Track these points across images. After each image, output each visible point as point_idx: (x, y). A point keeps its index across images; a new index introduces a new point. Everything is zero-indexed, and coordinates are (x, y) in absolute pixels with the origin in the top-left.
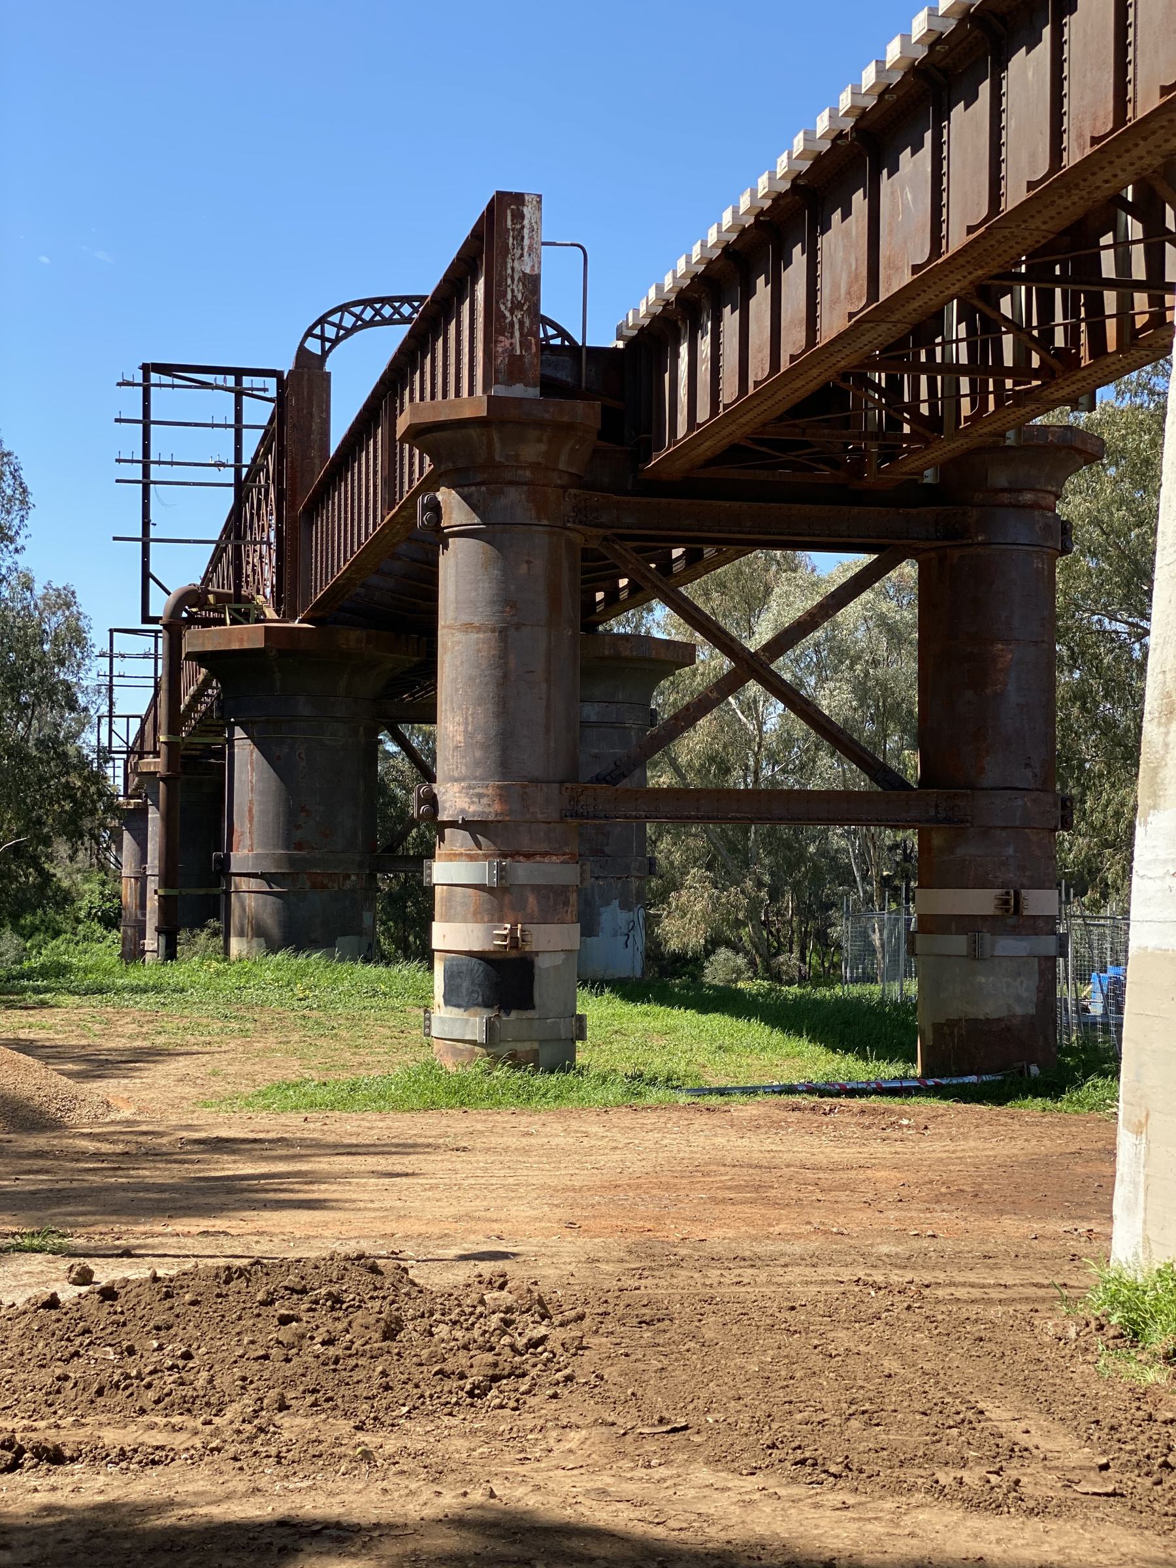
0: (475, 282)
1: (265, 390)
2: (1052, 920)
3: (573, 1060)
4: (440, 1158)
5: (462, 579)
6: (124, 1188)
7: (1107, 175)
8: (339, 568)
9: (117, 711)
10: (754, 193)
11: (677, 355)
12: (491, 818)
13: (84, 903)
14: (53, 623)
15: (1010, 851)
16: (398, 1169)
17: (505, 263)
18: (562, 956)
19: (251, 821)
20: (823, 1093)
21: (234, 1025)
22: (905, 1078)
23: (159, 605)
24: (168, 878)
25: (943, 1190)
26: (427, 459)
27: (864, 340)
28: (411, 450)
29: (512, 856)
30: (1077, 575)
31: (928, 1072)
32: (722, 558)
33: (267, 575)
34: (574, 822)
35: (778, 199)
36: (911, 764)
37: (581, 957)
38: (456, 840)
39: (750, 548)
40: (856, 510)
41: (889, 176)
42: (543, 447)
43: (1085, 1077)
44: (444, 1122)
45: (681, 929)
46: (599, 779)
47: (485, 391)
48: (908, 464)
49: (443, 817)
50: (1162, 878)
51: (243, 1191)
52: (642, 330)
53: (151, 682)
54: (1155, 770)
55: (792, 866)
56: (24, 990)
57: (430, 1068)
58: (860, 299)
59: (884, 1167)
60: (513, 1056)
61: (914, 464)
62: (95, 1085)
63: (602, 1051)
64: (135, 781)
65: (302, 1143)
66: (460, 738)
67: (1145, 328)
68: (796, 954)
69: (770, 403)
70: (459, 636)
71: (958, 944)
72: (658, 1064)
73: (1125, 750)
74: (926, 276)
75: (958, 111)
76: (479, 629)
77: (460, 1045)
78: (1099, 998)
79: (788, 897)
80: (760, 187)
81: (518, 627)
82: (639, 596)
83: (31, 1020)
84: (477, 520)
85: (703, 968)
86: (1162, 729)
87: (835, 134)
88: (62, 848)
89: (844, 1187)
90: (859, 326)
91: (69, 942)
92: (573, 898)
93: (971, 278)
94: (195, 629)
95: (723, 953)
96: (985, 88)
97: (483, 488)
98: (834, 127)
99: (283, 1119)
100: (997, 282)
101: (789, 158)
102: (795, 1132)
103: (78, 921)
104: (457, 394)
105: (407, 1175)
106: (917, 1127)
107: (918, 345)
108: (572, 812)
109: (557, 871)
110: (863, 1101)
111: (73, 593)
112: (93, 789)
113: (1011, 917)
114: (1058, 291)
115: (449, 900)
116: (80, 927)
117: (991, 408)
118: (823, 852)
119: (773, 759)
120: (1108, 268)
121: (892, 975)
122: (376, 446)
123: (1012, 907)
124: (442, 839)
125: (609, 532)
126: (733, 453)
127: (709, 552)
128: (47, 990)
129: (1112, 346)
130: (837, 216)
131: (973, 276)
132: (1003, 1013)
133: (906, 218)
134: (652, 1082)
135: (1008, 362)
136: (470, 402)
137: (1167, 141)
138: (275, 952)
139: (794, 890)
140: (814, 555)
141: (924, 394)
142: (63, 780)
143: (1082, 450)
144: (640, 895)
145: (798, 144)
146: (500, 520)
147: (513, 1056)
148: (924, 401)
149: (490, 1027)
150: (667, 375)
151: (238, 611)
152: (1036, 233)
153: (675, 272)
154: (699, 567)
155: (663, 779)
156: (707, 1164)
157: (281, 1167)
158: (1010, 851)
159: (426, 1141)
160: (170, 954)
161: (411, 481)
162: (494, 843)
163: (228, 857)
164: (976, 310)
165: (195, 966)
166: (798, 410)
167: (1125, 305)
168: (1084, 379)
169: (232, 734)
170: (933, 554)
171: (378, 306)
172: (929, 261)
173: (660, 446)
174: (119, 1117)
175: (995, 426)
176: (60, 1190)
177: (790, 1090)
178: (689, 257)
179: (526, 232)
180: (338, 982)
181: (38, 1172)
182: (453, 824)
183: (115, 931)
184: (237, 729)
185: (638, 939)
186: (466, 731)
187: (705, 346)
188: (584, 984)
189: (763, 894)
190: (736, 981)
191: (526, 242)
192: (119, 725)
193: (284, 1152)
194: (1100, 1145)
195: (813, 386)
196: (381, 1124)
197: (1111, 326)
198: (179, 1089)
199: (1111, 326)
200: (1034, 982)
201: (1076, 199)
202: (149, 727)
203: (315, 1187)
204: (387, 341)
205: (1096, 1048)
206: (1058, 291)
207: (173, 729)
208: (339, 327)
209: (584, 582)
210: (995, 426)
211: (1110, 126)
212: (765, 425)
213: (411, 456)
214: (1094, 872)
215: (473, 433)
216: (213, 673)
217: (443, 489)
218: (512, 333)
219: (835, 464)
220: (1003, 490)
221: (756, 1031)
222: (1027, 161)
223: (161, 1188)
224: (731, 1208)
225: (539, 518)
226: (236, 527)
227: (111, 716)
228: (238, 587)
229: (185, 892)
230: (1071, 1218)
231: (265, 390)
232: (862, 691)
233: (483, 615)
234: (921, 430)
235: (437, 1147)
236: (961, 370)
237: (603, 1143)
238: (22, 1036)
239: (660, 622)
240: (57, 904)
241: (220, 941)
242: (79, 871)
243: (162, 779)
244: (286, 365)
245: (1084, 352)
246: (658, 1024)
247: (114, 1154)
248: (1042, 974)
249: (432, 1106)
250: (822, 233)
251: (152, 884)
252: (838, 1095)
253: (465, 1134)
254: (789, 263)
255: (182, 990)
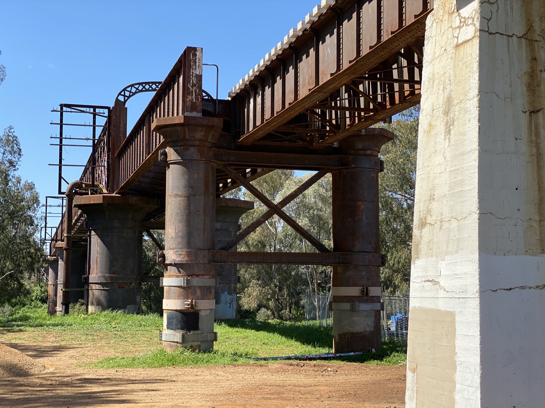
0: (179, 77)
1: (104, 113)
2: (379, 298)
3: (213, 348)
4: (165, 384)
5: (174, 179)
6: (51, 397)
7: (396, 44)
8: (130, 175)
9: (48, 226)
10: (276, 48)
11: (250, 103)
12: (184, 262)
13: (35, 294)
14: (28, 195)
15: (364, 273)
16: (150, 388)
17: (190, 71)
18: (209, 311)
19: (97, 264)
20: (300, 359)
21: (90, 337)
22: (329, 353)
23: (65, 188)
24: (66, 284)
25: (344, 393)
26: (162, 137)
27: (314, 98)
28: (156, 134)
29: (191, 276)
30: (386, 179)
31: (337, 351)
32: (264, 172)
33: (104, 177)
34: (214, 264)
35: (284, 51)
36: (329, 243)
37: (215, 311)
38: (172, 270)
39: (273, 169)
40: (310, 156)
41: (322, 44)
42: (203, 133)
43: (391, 353)
44: (167, 371)
45: (248, 302)
46: (222, 249)
47: (182, 114)
48: (328, 140)
49: (167, 262)
50: (420, 282)
51: (94, 397)
52: (237, 94)
53: (61, 215)
54: (418, 245)
55: (286, 280)
56: (13, 326)
57: (162, 351)
58: (313, 84)
59: (323, 386)
60: (191, 347)
61: (330, 141)
62: (40, 360)
63: (222, 345)
64: (54, 250)
65: (115, 380)
66: (173, 234)
67: (408, 96)
68: (288, 310)
69: (282, 119)
70: (173, 199)
71: (346, 306)
72: (242, 350)
73: (405, 238)
74: (335, 77)
75: (345, 22)
76: (180, 196)
77: (172, 343)
78: (395, 324)
79: (285, 290)
80: (278, 47)
81: (194, 195)
82: (235, 184)
83: (16, 336)
84: (180, 158)
85: (256, 315)
86: (420, 231)
87: (303, 29)
88: (26, 275)
89: (309, 393)
90: (313, 93)
91: (29, 308)
92: (213, 291)
93: (350, 78)
94: (77, 196)
95: (263, 310)
96: (355, 15)
97: (182, 148)
98: (295, 33)
99: (108, 371)
100: (359, 80)
101: (288, 37)
102: (291, 373)
103: (32, 301)
104: (173, 115)
105: (153, 390)
106: (333, 371)
107: (331, 100)
108: (213, 261)
109: (207, 281)
110: (315, 362)
111: (34, 185)
112: (39, 253)
113: (365, 296)
114: (379, 83)
115: (169, 292)
116: (33, 303)
117: (357, 122)
118: (297, 274)
119: (281, 242)
120: (395, 75)
121: (322, 317)
122: (143, 134)
123: (365, 293)
124: (167, 270)
125: (225, 163)
126: (269, 136)
127: (259, 170)
128: (22, 325)
129: (397, 101)
130: (304, 57)
131: (350, 78)
132: (362, 330)
133: (328, 59)
134: (241, 356)
135: (362, 106)
136: (178, 118)
137: (416, 33)
138: (104, 310)
139: (287, 288)
140: (295, 171)
141: (334, 117)
142: (28, 250)
143: (386, 137)
144: (235, 289)
145: (291, 32)
146: (188, 158)
147: (191, 347)
148: (397, 92)
149: (183, 336)
150: (246, 110)
151: (93, 190)
152: (372, 63)
153: (249, 75)
154: (256, 175)
155: (242, 249)
156: (261, 385)
157: (108, 389)
158: (364, 273)
159: (160, 378)
160: (67, 312)
161: (156, 145)
162: (185, 271)
163: (88, 277)
164: (351, 89)
165: (76, 316)
166: (291, 122)
167: (401, 89)
168: (388, 112)
169: (90, 233)
170: (337, 171)
171: (144, 85)
172: (336, 72)
173: (244, 134)
174: (49, 371)
175: (358, 128)
176: (27, 398)
177: (289, 358)
178: (254, 70)
179: (197, 60)
180: (124, 320)
181: (20, 391)
182: (171, 265)
183: (45, 304)
184: (92, 231)
185: (234, 305)
186: (175, 232)
187: (259, 99)
188: (215, 321)
189: (277, 289)
190: (268, 319)
191: (197, 64)
192: (49, 230)
193: (109, 383)
194: (397, 376)
195: (297, 113)
196: (144, 373)
197: (397, 95)
198: (70, 361)
199: (397, 95)
200: (373, 319)
201: (386, 52)
202: (59, 231)
203: (121, 396)
204: (148, 97)
205: (394, 342)
206: (379, 83)
207: (69, 232)
208: (130, 92)
209: (217, 180)
210: (358, 128)
211: (397, 28)
212: (280, 126)
213: (156, 136)
214: (391, 281)
215: (179, 128)
216: (84, 212)
217: (168, 148)
218: (192, 95)
219: (304, 140)
220: (361, 150)
221: (276, 337)
222: (369, 39)
223: (65, 397)
224: (270, 401)
225: (201, 158)
226: (93, 161)
227: (46, 227)
228: (93, 182)
229: (72, 289)
230: (388, 403)
231: (104, 113)
232: (312, 219)
233: (181, 191)
234: (333, 129)
235: (164, 380)
236: (346, 109)
237: (223, 378)
238: (13, 342)
239: (243, 194)
240: (25, 294)
241: (84, 307)
242: (33, 282)
243: (65, 249)
244: (112, 105)
245: (388, 103)
246: (241, 335)
247: (47, 384)
248: (375, 316)
249: (162, 365)
250: (300, 62)
251: (60, 287)
252: (306, 360)
253: (174, 376)
254: (288, 72)
255: (71, 325)
